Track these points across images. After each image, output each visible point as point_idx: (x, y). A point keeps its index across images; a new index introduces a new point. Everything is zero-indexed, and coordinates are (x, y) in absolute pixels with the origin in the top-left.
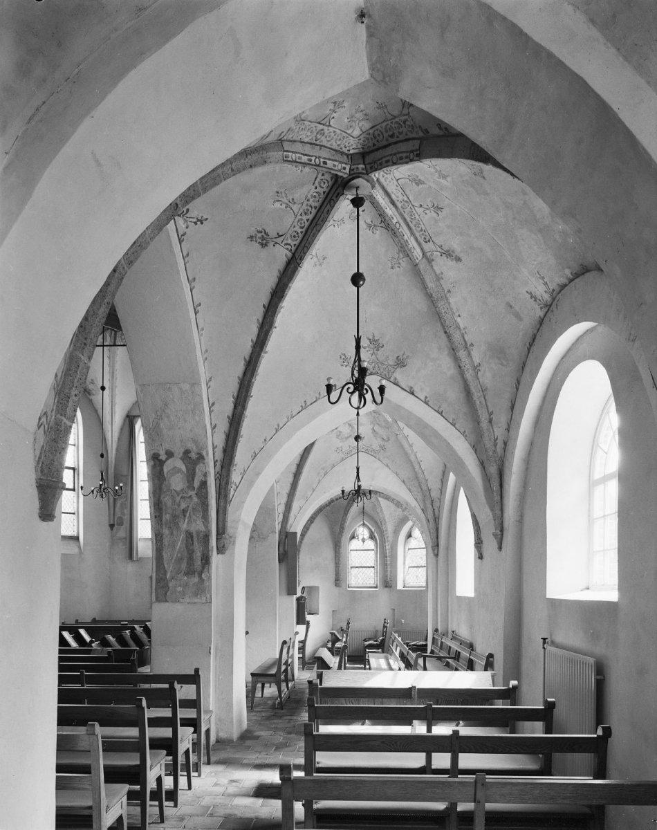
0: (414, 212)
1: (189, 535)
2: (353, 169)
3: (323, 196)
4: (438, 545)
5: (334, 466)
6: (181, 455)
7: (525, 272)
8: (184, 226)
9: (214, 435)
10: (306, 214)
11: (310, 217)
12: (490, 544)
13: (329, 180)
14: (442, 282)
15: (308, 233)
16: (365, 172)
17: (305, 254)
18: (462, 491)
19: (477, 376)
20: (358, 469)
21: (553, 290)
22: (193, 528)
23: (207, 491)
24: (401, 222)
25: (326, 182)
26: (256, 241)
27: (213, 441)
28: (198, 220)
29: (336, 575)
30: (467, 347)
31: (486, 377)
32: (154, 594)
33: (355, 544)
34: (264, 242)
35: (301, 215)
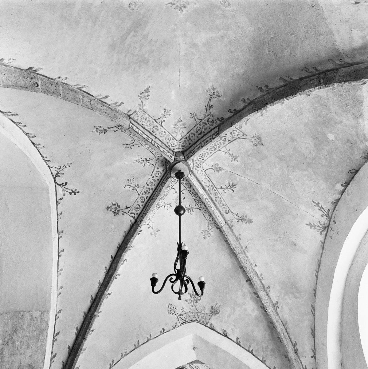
0: (217, 193)
2: (177, 159)
3: (157, 182)
7: (303, 207)
8: (62, 193)
9: (53, 364)
10: (146, 193)
11: (149, 195)
13: (162, 172)
14: (240, 241)
15: (147, 205)
16: (184, 160)
17: (144, 218)
19: (277, 313)
21: (329, 210)
25: (160, 173)
26: (111, 211)
28: (73, 192)
30: (266, 289)
31: (285, 312)
34: (116, 211)
35: (143, 194)
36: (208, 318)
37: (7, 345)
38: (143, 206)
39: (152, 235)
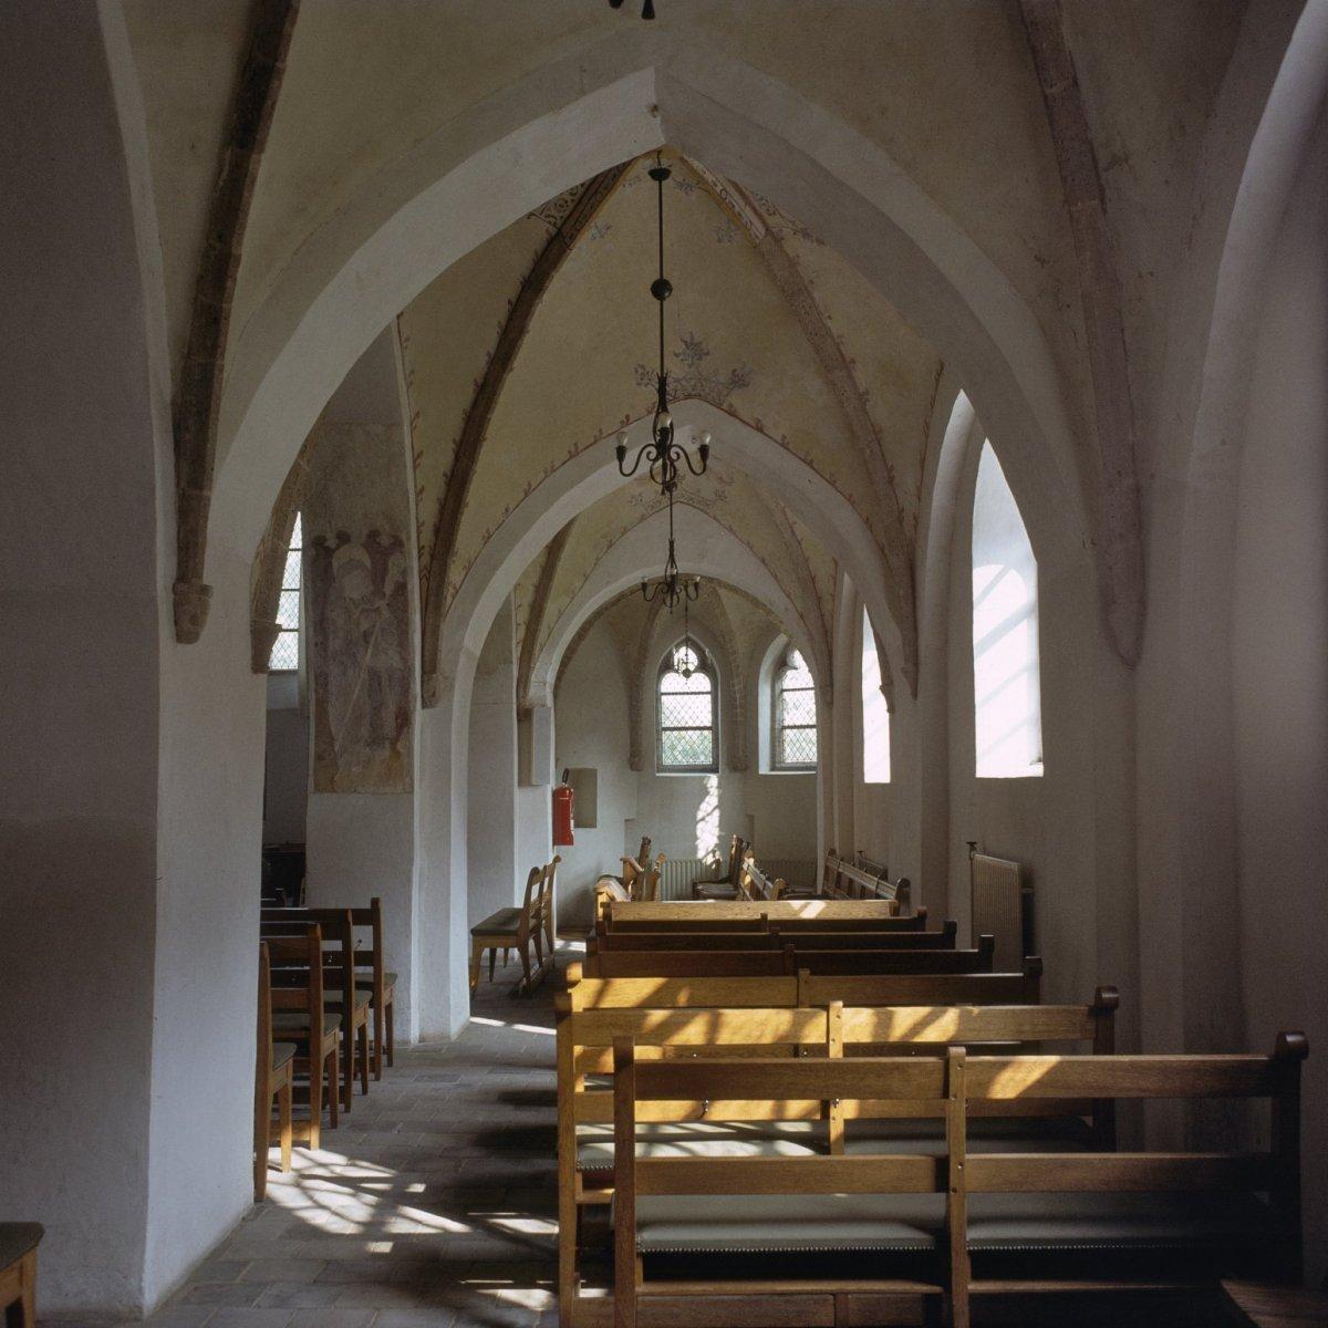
1: (374, 675)
4: (832, 685)
5: (625, 531)
12: (903, 686)
18: (989, 462)
20: (672, 543)
23: (406, 600)
24: (731, 190)
27: (419, 515)
29: (632, 746)
33: (670, 682)
36: (725, 393)
38: (575, 203)
39: (595, 238)
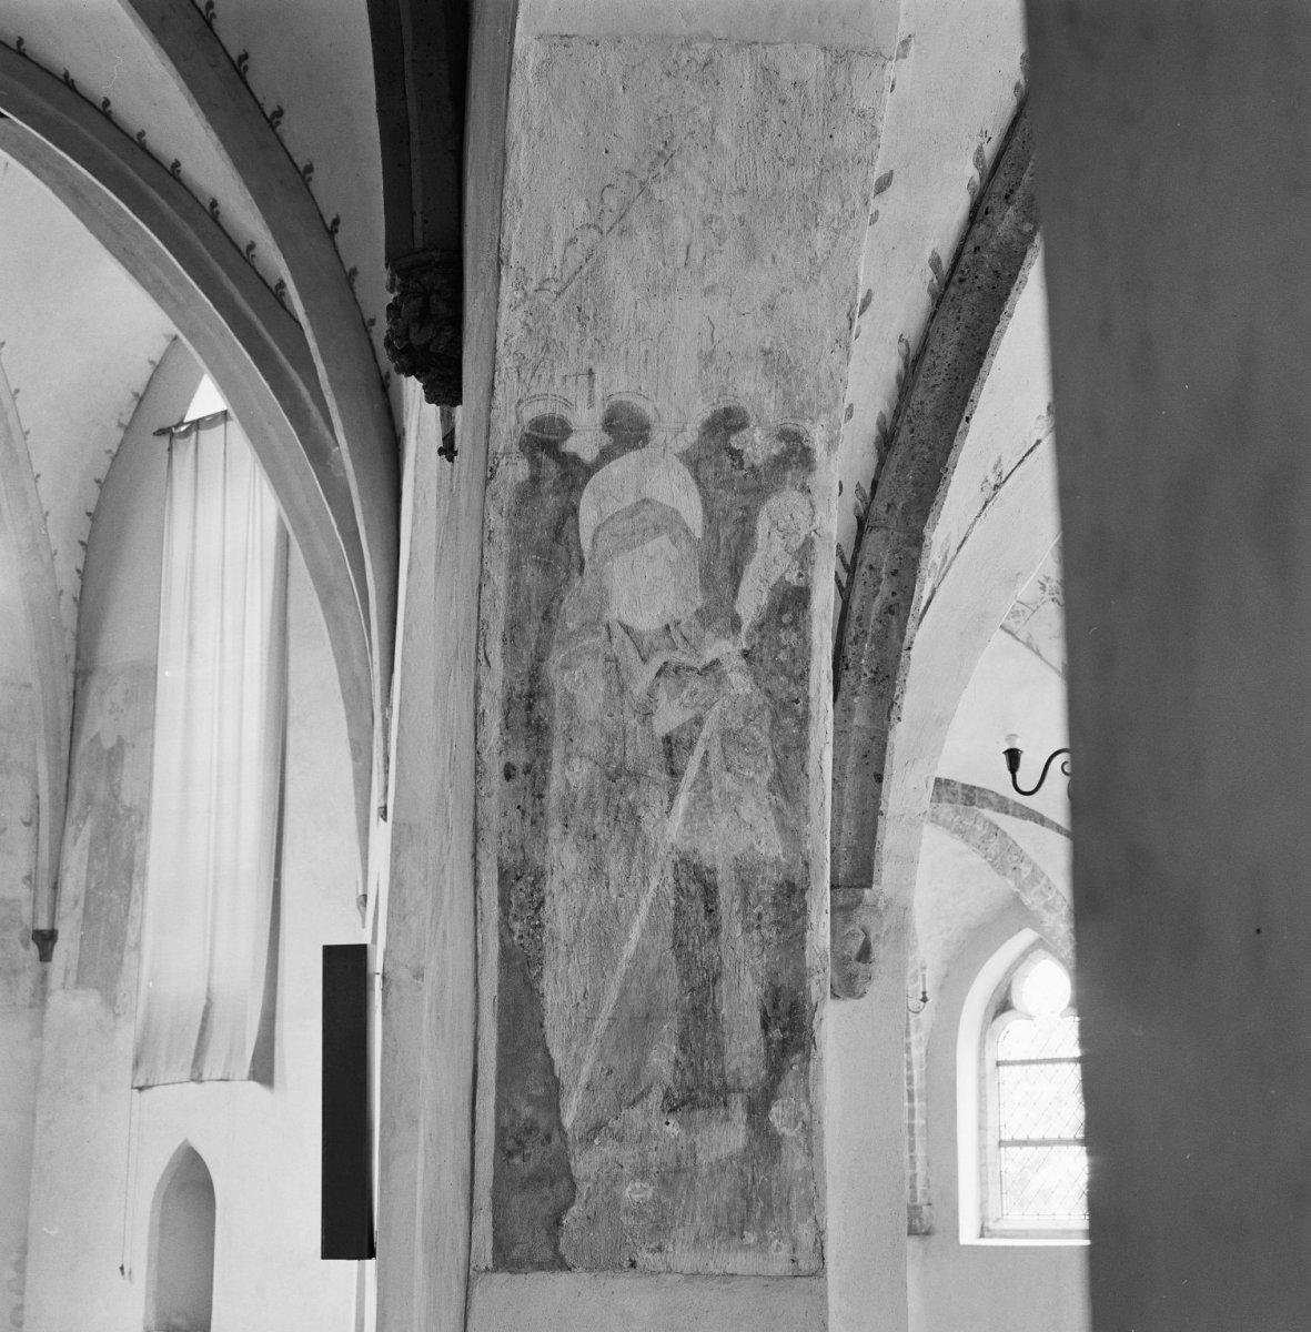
6: (691, 436)
22: (719, 847)
32: (484, 1222)
37: (622, 232)
